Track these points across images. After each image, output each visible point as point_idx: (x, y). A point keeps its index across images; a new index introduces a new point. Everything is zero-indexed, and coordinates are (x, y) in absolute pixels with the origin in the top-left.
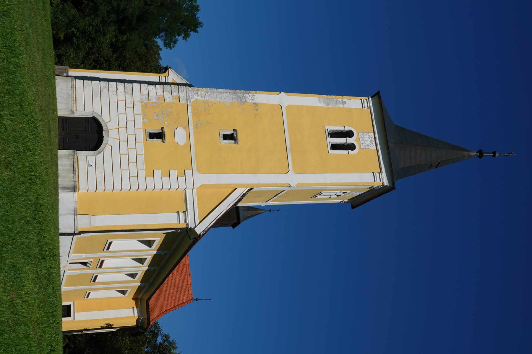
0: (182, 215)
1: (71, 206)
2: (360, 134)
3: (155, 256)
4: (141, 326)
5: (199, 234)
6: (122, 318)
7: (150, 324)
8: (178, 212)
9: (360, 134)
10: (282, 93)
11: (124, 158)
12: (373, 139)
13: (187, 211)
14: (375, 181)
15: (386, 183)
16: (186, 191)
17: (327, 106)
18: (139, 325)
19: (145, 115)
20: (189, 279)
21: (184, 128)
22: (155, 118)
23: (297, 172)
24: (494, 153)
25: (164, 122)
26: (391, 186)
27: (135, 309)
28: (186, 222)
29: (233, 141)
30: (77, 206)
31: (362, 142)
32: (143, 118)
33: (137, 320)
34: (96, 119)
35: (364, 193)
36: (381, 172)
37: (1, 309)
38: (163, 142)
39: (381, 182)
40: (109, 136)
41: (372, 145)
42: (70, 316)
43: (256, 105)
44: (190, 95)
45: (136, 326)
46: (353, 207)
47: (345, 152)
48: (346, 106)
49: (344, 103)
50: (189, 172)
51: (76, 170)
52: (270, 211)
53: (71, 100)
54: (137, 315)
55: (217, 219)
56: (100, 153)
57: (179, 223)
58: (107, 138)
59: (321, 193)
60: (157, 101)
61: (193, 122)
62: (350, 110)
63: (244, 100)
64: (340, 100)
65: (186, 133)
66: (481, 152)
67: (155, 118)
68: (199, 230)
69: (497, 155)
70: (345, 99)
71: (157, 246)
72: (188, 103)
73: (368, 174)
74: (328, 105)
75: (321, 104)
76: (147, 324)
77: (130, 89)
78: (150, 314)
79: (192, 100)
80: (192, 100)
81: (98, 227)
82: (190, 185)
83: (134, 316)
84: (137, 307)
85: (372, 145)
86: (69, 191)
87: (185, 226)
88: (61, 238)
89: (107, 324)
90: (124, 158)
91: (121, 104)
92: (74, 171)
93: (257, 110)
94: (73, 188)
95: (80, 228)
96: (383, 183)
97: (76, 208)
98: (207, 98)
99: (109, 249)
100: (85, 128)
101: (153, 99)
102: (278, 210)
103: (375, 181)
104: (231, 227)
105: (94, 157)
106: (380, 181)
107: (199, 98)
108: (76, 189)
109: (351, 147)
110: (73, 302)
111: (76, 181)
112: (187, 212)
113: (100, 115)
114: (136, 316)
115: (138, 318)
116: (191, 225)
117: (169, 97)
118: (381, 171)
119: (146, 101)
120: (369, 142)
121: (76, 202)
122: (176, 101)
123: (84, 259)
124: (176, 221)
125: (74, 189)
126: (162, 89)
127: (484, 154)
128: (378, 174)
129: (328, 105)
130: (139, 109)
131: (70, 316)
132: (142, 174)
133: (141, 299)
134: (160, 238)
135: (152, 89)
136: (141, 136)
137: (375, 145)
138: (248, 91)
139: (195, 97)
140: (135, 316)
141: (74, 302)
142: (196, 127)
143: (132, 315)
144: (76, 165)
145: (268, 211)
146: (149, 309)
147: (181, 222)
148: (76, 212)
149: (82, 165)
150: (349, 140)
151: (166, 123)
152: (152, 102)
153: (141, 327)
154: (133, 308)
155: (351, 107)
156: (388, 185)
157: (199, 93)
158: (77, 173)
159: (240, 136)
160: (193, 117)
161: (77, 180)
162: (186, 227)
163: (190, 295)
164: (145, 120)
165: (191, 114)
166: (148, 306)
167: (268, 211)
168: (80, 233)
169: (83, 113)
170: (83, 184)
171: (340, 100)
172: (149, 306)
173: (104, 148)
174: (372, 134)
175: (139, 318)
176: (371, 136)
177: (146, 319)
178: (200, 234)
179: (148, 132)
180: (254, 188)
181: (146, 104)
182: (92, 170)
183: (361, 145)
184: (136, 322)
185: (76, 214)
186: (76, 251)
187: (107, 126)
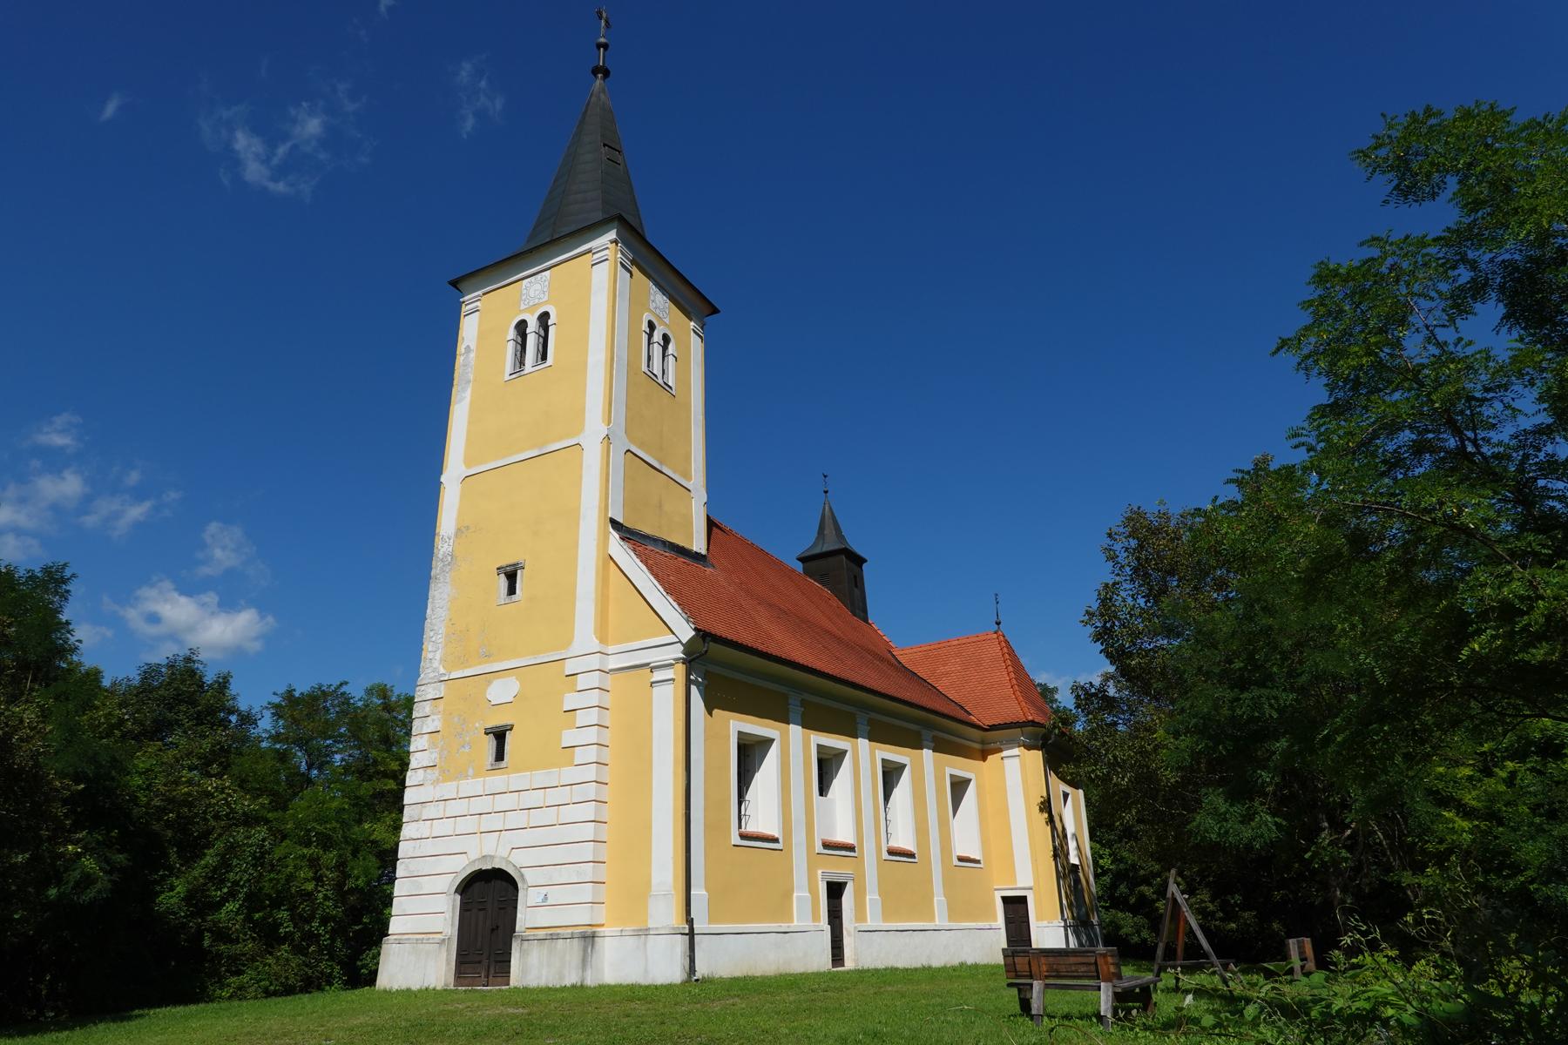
0: (658, 676)
1: (631, 941)
2: (523, 307)
3: (806, 725)
5: (693, 633)
6: (1025, 781)
7: (1033, 721)
8: (1002, 759)
9: (523, 307)
10: (442, 479)
11: (538, 817)
12: (532, 279)
13: (648, 664)
14: (607, 260)
15: (612, 235)
16: (611, 670)
17: (471, 384)
19: (461, 775)
20: (957, 642)
21: (490, 682)
22: (467, 750)
23: (580, 428)
24: (599, 46)
25: (476, 728)
26: (616, 223)
27: (1005, 753)
28: (672, 665)
29: (519, 572)
30: (629, 928)
31: (537, 301)
32: (466, 777)
33: (1029, 748)
34: (470, 880)
35: (657, 284)
36: (590, 252)
38: (511, 730)
39: (609, 246)
40: (493, 854)
41: (544, 278)
42: (1026, 897)
43: (459, 531)
44: (432, 675)
46: (715, 311)
47: (552, 330)
48: (473, 347)
49: (468, 349)
50: (570, 667)
51: (551, 934)
52: (826, 492)
53: (421, 946)
54: (1017, 749)
55: (665, 593)
56: (522, 876)
57: (673, 680)
58: (496, 860)
59: (653, 376)
61: (480, 664)
62: (482, 336)
63: (449, 558)
64: (462, 358)
65: (498, 678)
66: (595, 71)
67: (467, 750)
68: (686, 632)
69: (602, 40)
70: (461, 348)
71: (767, 726)
72: (446, 678)
73: (594, 275)
74: (469, 381)
75: (465, 397)
77: (413, 809)
78: (1012, 723)
79: (442, 671)
80: (442, 671)
81: (675, 876)
82: (594, 661)
84: (1000, 750)
85: (544, 278)
86: (592, 951)
87: (681, 668)
88: (702, 970)
89: (1041, 810)
90: (538, 817)
91: (440, 828)
92: (554, 938)
93: (468, 528)
94: (585, 941)
95: (677, 920)
96: (612, 243)
97: (634, 930)
98: (440, 638)
99: (777, 836)
100: (480, 910)
101: (433, 756)
102: (825, 476)
103: (607, 260)
105: (530, 889)
106: (607, 248)
107: (438, 656)
108: (586, 932)
109: (544, 318)
111: (572, 933)
112: (652, 665)
113: (455, 877)
115: (1022, 748)
116: (677, 652)
117: (433, 720)
118: (589, 251)
119: (436, 771)
120: (538, 287)
121: (622, 931)
122: (441, 704)
123: (813, 890)
124: (669, 688)
125: (589, 938)
126: (418, 738)
127: (601, 64)
128: (596, 256)
129: (469, 381)
130: (448, 789)
131: (1026, 897)
132: (569, 774)
133: (983, 742)
134: (729, 722)
135: (416, 759)
136: (497, 781)
137: (543, 274)
138: (435, 551)
139: (436, 664)
140: (1018, 753)
142: (489, 656)
143: (1017, 760)
144: (541, 933)
145: (826, 497)
146: (1000, 724)
147: (672, 676)
148: (641, 930)
149: (543, 918)
150: (532, 325)
151: (477, 725)
152: (440, 758)
153: (1034, 736)
154: (1002, 759)
155: (476, 335)
156: (615, 230)
157: (430, 656)
158: (559, 931)
159: (506, 561)
160: (470, 666)
161: (569, 931)
162: (683, 663)
163: (989, 637)
164: (470, 772)
165: (465, 671)
166: (993, 728)
167: (826, 497)
168: (690, 922)
169: (447, 916)
170: (581, 917)
171: (462, 358)
172: (994, 725)
173: (514, 866)
174: (525, 282)
176: (529, 285)
178: (695, 629)
179: (492, 765)
180: (610, 516)
181: (443, 771)
182: (556, 895)
183: (541, 301)
184: (1032, 751)
185: (647, 930)
186: (784, 911)
187: (474, 861)
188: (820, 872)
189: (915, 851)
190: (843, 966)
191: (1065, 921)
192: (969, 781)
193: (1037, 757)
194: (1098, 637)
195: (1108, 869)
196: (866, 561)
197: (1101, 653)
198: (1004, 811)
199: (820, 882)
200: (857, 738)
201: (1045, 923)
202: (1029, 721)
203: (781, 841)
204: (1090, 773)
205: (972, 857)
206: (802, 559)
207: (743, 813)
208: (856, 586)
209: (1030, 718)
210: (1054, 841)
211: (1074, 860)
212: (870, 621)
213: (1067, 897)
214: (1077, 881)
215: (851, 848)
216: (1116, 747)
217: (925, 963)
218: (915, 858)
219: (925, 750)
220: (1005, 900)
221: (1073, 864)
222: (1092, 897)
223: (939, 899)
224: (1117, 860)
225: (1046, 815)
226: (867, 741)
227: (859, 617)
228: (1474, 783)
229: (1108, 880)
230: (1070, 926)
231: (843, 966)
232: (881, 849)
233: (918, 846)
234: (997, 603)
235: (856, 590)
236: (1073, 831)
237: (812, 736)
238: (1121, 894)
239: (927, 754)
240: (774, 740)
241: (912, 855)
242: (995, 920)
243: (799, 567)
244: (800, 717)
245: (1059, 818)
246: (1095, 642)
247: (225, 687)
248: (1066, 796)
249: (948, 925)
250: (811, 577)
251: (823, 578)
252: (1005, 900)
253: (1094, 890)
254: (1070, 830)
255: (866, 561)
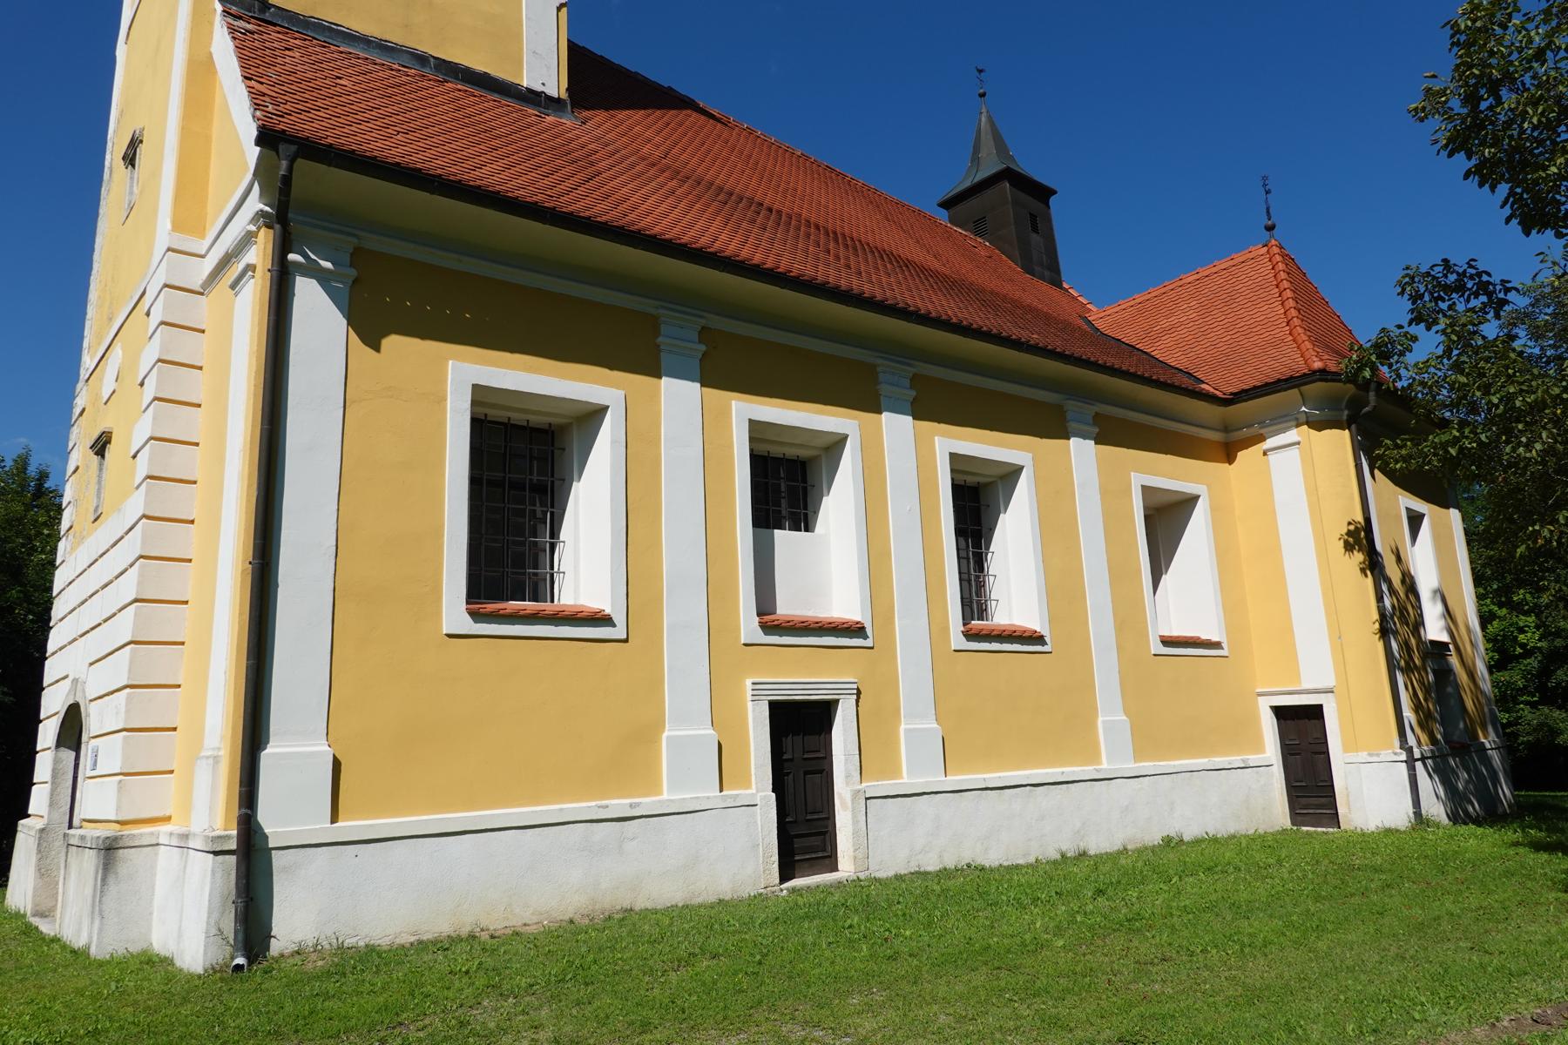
4: (1347, 407)
7: (1323, 371)
8: (1265, 454)
18: (1345, 418)
27: (1270, 443)
33: (1319, 425)
37: (12, 1043)
42: (1320, 707)
45: (1353, 426)
60: (1536, 653)
76: (1326, 380)
78: (1279, 380)
83: (1298, 443)
84: (1262, 438)
89: (1349, 547)
104: (1053, 200)
110: (1260, 699)
114: (1299, 435)
115: (1305, 427)
131: (1320, 707)
133: (1226, 429)
141: (1260, 694)
143: (1294, 451)
153: (1331, 402)
154: (1265, 454)
175: (1305, 420)
177: (1303, 388)
188: (748, 682)
189: (1045, 632)
190: (835, 868)
191: (1410, 751)
192: (1192, 500)
193: (1340, 441)
194: (1458, 143)
195: (1535, 648)
196: (1054, 192)
197: (1466, 177)
198: (1271, 550)
199: (750, 704)
200: (880, 412)
201: (1363, 756)
202: (1314, 372)
203: (869, 631)
204: (1444, 446)
205: (1204, 637)
206: (946, 204)
207: (556, 569)
208: (1035, 230)
209: (1317, 365)
210: (1380, 599)
211: (1435, 630)
212: (1065, 285)
213: (1417, 707)
214: (1444, 673)
215: (857, 630)
216: (1509, 376)
217: (1070, 848)
218: (865, 637)
219: (1072, 439)
220: (1281, 713)
221: (1433, 642)
222: (1483, 701)
223: (1110, 717)
224: (1551, 634)
225: (1359, 557)
226: (908, 420)
227: (1042, 278)
228: (432, 1006)
229: (1536, 664)
230: (1423, 759)
231: (835, 868)
232: (946, 629)
233: (1052, 620)
234: (1268, 192)
235: (1034, 235)
236: (1435, 584)
237: (733, 402)
238: (1558, 684)
239: (1081, 452)
240: (606, 408)
241: (1038, 639)
242: (1259, 747)
243: (942, 216)
244: (697, 363)
245: (1393, 558)
246: (1450, 155)
247: (26, 469)
248: (1415, 520)
249: (1131, 767)
250: (956, 226)
251: (979, 226)
252: (1281, 713)
253: (1486, 685)
254: (1427, 581)
255: (1054, 192)
